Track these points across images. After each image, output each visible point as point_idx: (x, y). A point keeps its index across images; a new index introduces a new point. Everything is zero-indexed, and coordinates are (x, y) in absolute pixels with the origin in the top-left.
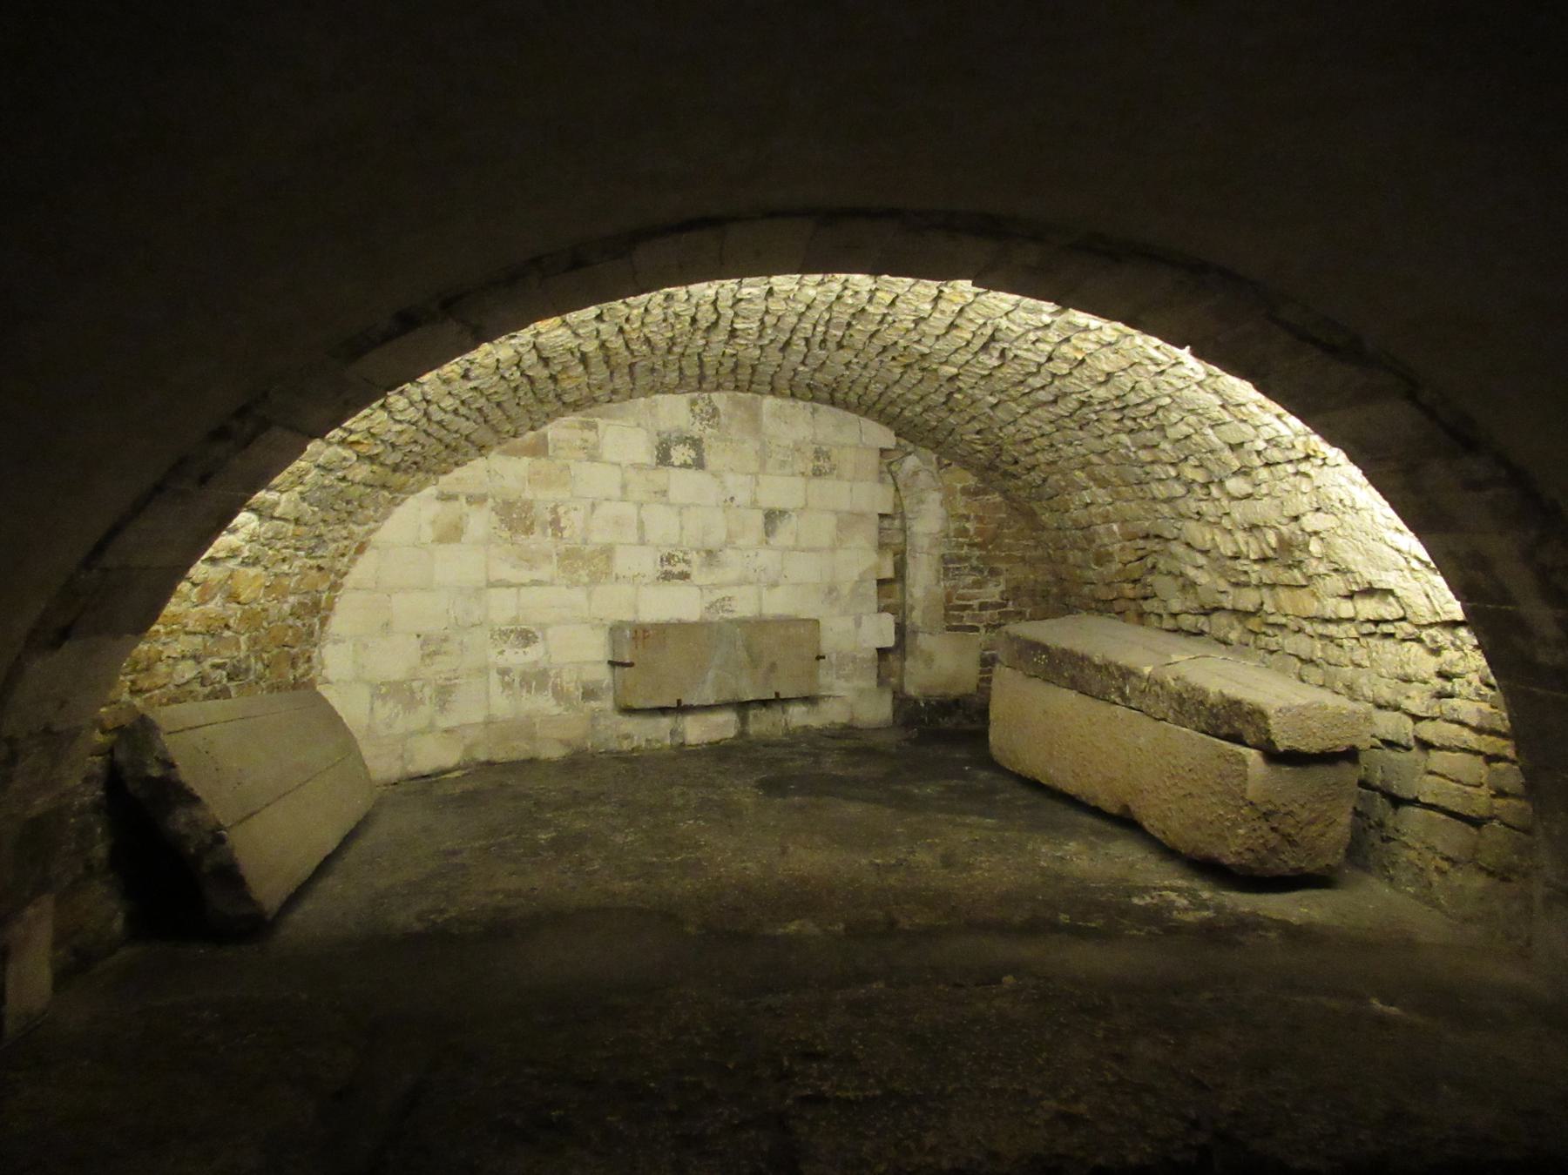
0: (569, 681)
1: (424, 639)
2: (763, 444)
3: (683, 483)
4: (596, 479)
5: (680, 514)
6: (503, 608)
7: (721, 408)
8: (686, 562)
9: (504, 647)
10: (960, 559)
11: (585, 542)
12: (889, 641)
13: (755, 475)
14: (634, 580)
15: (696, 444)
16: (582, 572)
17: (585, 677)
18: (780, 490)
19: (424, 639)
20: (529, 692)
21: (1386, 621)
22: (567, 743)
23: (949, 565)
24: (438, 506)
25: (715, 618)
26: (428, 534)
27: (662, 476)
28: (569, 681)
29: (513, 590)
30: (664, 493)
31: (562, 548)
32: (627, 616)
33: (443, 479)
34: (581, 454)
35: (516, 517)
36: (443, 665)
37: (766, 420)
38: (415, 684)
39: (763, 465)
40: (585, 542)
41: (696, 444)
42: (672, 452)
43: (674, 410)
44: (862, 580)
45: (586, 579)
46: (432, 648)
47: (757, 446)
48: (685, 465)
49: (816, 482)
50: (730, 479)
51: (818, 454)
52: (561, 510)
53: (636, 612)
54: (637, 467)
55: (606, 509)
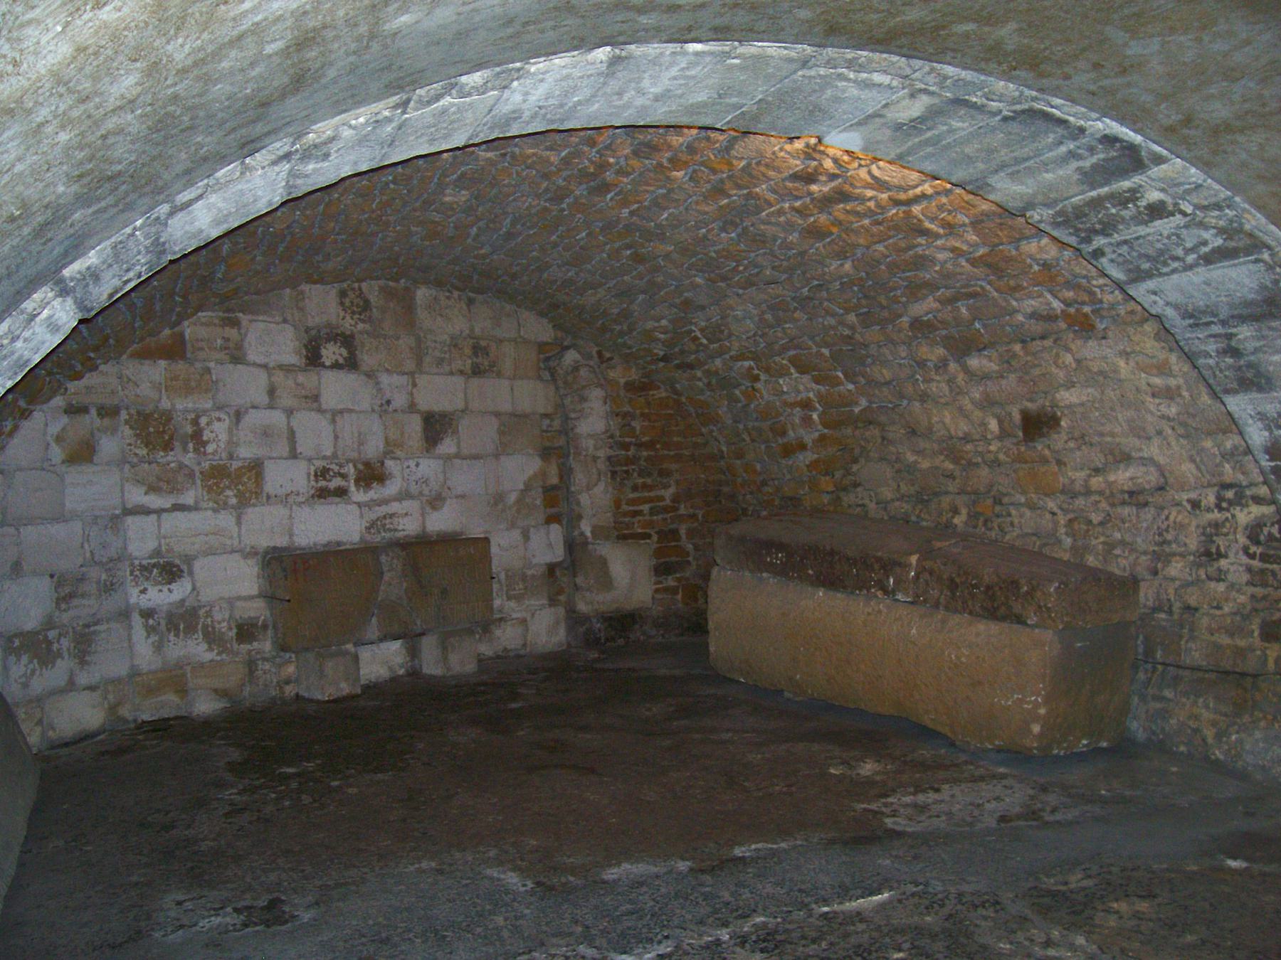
0: (222, 620)
1: (60, 580)
2: (419, 341)
3: (336, 387)
4: (244, 384)
5: (334, 421)
6: (141, 538)
7: (373, 299)
8: (344, 476)
9: (146, 585)
10: (630, 461)
11: (231, 457)
12: (558, 554)
13: (411, 374)
14: (285, 500)
15: (347, 341)
16: (229, 493)
17: (237, 614)
18: (440, 391)
19: (60, 580)
20: (177, 635)
21: (123, 211)
22: (221, 693)
23: (618, 470)
24: (65, 420)
25: (377, 538)
26: (57, 453)
27: (308, 379)
28: (222, 620)
29: (154, 517)
30: (316, 398)
31: (206, 465)
32: (282, 542)
33: (72, 386)
34: (221, 356)
35: (155, 431)
36: (84, 608)
37: (422, 314)
38: (52, 634)
39: (419, 362)
40: (231, 457)
41: (347, 341)
42: (324, 352)
43: (323, 305)
44: (528, 487)
45: (234, 501)
46: (67, 590)
47: (412, 341)
48: (336, 366)
49: (475, 382)
50: (385, 379)
51: (476, 350)
52: (203, 421)
53: (291, 535)
54: (287, 369)
55: (253, 419)
